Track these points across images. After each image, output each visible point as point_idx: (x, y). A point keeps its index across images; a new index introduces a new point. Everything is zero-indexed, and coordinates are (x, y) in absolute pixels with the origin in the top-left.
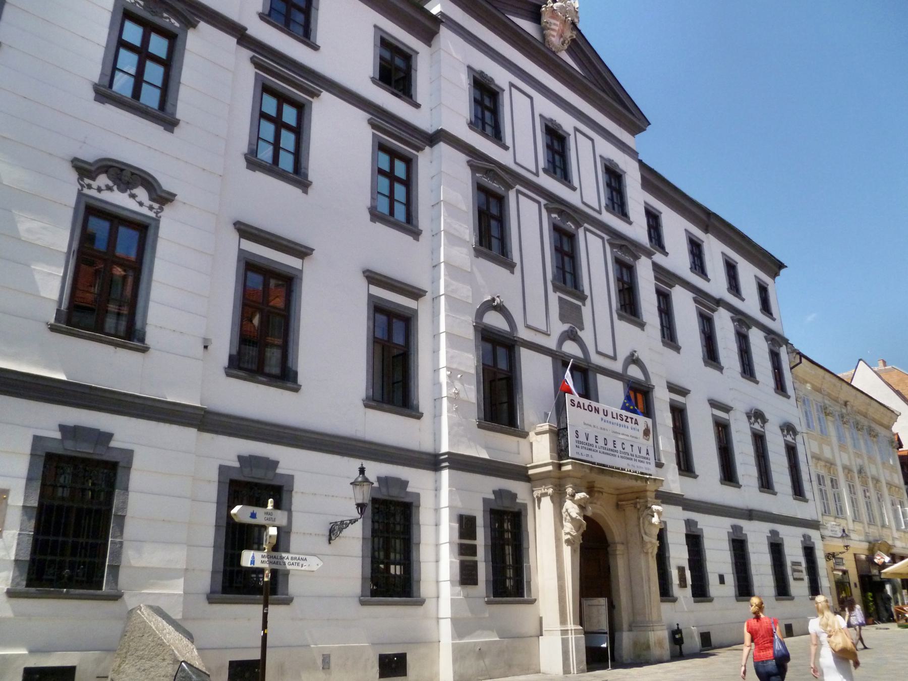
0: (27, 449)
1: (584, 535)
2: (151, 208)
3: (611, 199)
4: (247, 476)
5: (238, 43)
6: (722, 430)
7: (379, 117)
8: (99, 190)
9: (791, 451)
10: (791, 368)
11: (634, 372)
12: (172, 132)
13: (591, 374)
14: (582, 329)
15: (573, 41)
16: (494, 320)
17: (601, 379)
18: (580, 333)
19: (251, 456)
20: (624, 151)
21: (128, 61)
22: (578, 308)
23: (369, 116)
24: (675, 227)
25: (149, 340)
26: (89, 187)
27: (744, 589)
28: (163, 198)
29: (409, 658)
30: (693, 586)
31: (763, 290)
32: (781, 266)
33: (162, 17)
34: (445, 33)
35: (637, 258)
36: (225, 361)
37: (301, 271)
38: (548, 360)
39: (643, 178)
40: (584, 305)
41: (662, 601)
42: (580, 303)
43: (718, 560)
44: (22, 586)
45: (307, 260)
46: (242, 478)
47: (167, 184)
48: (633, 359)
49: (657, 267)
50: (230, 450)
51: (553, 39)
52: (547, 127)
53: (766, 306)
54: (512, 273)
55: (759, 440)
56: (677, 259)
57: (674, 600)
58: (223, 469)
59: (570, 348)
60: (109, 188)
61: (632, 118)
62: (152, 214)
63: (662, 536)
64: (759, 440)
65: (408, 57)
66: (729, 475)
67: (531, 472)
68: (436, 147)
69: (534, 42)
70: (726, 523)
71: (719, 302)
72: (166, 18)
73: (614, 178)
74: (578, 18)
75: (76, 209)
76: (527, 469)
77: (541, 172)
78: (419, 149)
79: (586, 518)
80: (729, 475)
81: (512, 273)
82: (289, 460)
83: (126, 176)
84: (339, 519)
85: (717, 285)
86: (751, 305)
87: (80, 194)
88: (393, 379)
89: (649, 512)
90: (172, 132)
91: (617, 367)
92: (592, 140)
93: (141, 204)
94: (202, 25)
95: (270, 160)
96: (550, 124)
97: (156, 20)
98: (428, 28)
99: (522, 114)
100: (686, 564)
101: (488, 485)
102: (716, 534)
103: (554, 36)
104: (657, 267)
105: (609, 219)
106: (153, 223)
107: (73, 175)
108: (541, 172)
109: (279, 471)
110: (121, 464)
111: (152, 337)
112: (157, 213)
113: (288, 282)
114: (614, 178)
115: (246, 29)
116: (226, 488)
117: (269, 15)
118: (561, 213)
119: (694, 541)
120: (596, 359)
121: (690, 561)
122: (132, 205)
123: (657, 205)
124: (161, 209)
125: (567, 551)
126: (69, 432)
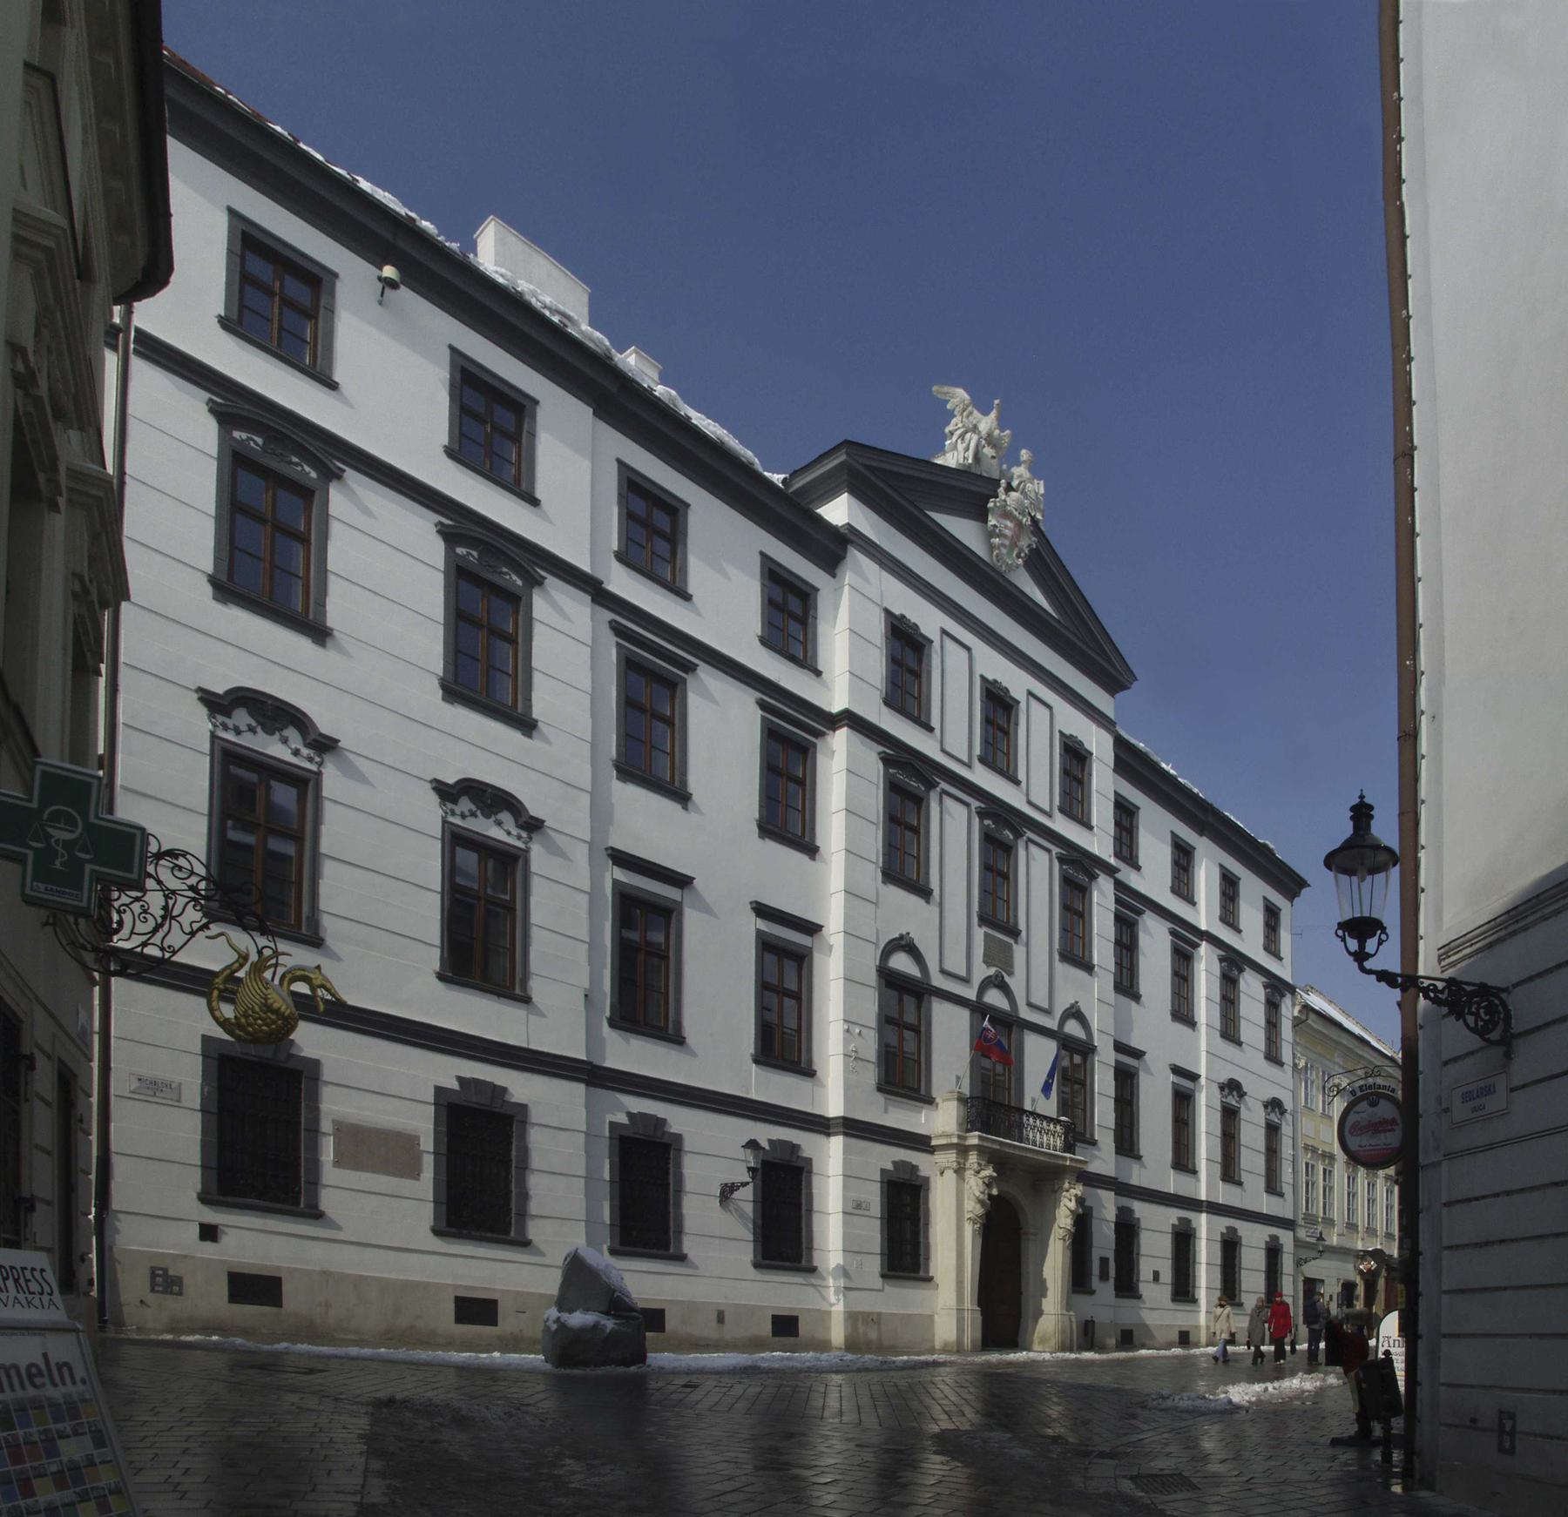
0: (197, 1047)
2: (519, 838)
3: (1065, 793)
7: (461, 526)
8: (238, 732)
9: (1272, 1130)
11: (1073, 1028)
14: (1011, 974)
18: (1007, 978)
22: (1009, 948)
23: (207, 395)
24: (1157, 830)
27: (1183, 1290)
34: (855, 557)
38: (965, 1014)
39: (1117, 758)
42: (1011, 941)
43: (1155, 1251)
44: (618, 1247)
45: (686, 891)
47: (325, 724)
48: (1075, 1013)
49: (1120, 886)
52: (988, 691)
57: (1092, 1292)
59: (994, 998)
60: (473, 814)
62: (314, 768)
64: (1230, 1116)
66: (1183, 1160)
67: (934, 1143)
70: (1172, 1215)
72: (297, 464)
73: (1074, 756)
76: (929, 1138)
79: (990, 1197)
80: (1229, 1171)
83: (276, 714)
85: (1204, 914)
91: (1052, 1024)
92: (968, 649)
93: (509, 833)
94: (351, 475)
98: (831, 548)
100: (1111, 1256)
102: (1156, 1225)
104: (1120, 886)
105: (1063, 826)
107: (434, 799)
114: (1074, 756)
117: (240, 321)
121: (1118, 1252)
122: (496, 833)
123: (1134, 795)
124: (530, 838)
125: (968, 1230)
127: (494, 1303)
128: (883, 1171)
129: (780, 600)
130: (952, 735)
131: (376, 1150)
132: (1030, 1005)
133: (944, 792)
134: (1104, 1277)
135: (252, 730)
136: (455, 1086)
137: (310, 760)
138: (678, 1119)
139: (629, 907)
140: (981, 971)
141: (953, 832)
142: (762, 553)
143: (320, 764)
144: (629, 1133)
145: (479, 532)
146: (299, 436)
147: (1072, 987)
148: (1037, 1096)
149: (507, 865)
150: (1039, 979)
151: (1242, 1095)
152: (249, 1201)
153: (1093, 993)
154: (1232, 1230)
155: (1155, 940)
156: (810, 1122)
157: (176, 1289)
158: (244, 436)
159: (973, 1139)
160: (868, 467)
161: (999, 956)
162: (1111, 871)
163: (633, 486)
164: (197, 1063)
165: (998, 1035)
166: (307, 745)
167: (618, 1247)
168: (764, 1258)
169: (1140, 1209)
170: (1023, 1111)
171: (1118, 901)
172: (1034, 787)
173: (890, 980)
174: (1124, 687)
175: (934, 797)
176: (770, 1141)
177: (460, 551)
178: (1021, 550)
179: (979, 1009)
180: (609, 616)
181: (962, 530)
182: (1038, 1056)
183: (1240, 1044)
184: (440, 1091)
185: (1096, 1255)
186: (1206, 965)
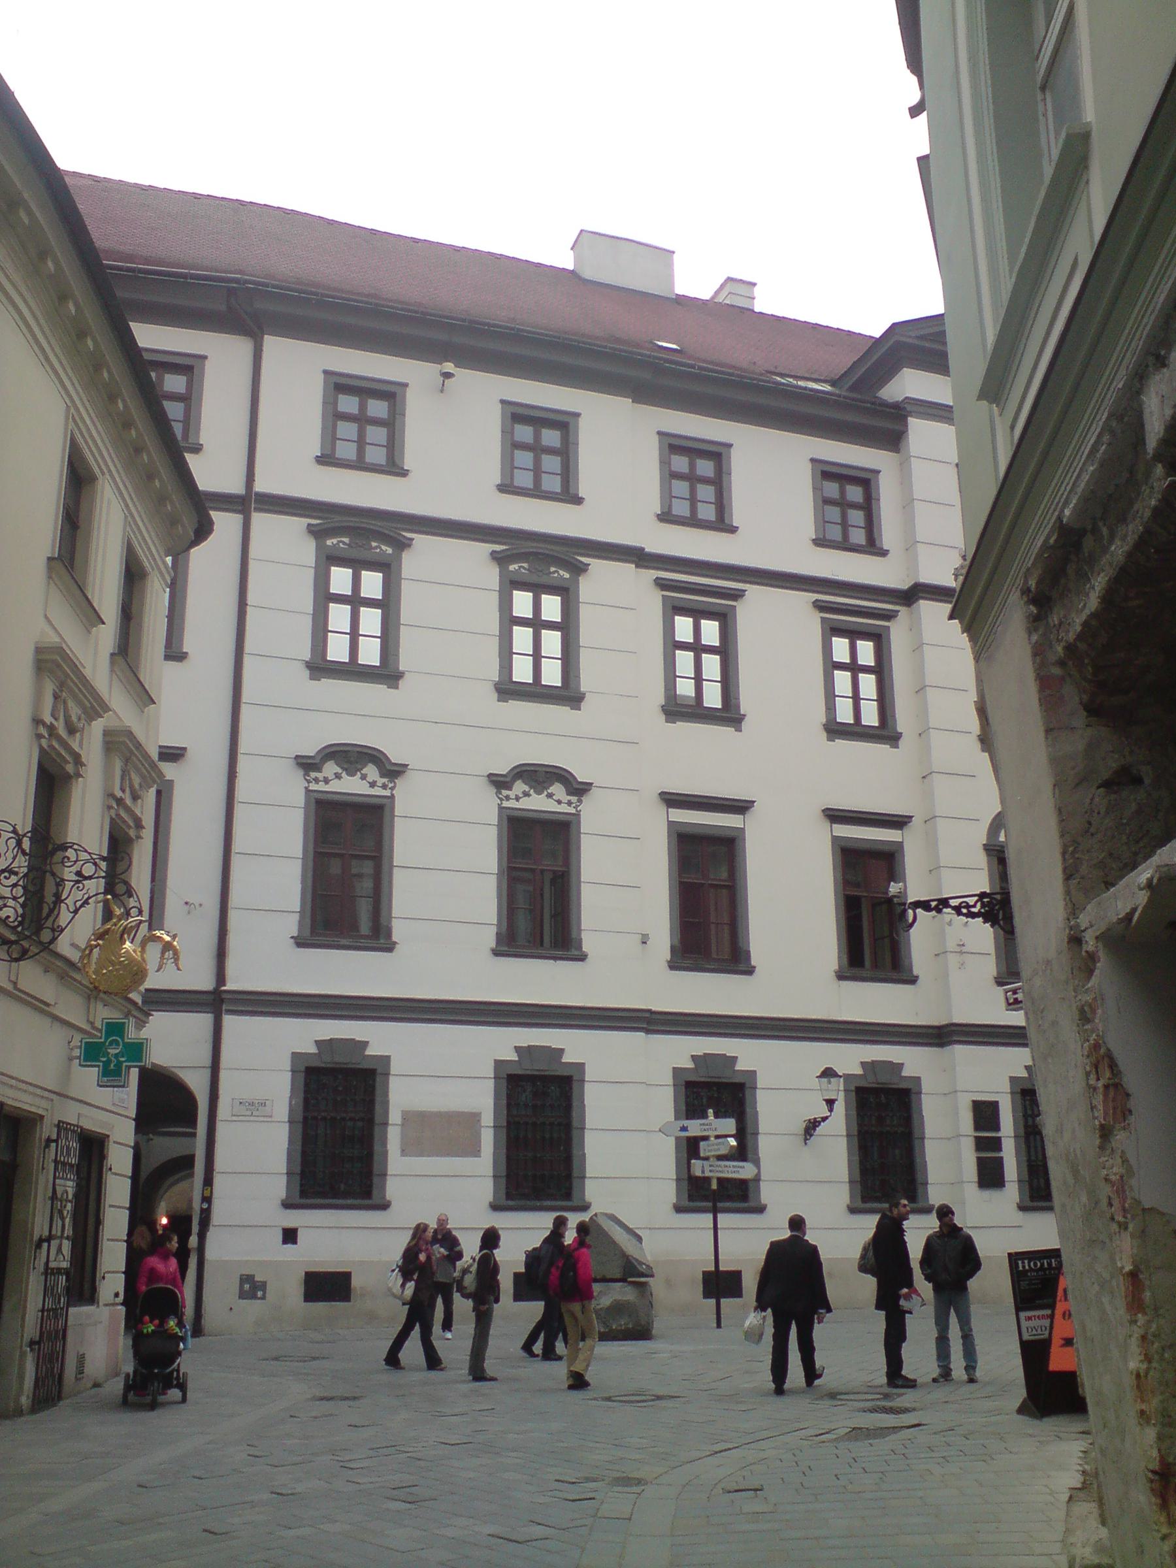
2: (569, 803)
4: (327, 1061)
5: (637, 567)
8: (326, 781)
12: (397, 688)
19: (873, 1062)
21: (684, 660)
25: (586, 948)
26: (508, 798)
28: (579, 790)
33: (371, 548)
34: (916, 425)
36: (667, 955)
37: (743, 830)
45: (905, 829)
47: (395, 756)
50: (683, 1051)
60: (526, 794)
62: (387, 793)
72: (554, 572)
78: (889, 616)
87: (501, 808)
90: (397, 688)
93: (559, 802)
97: (544, 580)
109: (739, 1067)
110: (379, 1071)
111: (589, 942)
113: (727, 848)
115: (643, 549)
116: (301, 1077)
124: (580, 801)
126: (870, 1067)
131: (444, 1133)
136: (691, 1065)
137: (384, 787)
142: (659, 433)
143: (392, 789)
145: (530, 547)
146: (375, 525)
152: (349, 1202)
157: (260, 1294)
158: (335, 541)
167: (686, 1203)
177: (512, 567)
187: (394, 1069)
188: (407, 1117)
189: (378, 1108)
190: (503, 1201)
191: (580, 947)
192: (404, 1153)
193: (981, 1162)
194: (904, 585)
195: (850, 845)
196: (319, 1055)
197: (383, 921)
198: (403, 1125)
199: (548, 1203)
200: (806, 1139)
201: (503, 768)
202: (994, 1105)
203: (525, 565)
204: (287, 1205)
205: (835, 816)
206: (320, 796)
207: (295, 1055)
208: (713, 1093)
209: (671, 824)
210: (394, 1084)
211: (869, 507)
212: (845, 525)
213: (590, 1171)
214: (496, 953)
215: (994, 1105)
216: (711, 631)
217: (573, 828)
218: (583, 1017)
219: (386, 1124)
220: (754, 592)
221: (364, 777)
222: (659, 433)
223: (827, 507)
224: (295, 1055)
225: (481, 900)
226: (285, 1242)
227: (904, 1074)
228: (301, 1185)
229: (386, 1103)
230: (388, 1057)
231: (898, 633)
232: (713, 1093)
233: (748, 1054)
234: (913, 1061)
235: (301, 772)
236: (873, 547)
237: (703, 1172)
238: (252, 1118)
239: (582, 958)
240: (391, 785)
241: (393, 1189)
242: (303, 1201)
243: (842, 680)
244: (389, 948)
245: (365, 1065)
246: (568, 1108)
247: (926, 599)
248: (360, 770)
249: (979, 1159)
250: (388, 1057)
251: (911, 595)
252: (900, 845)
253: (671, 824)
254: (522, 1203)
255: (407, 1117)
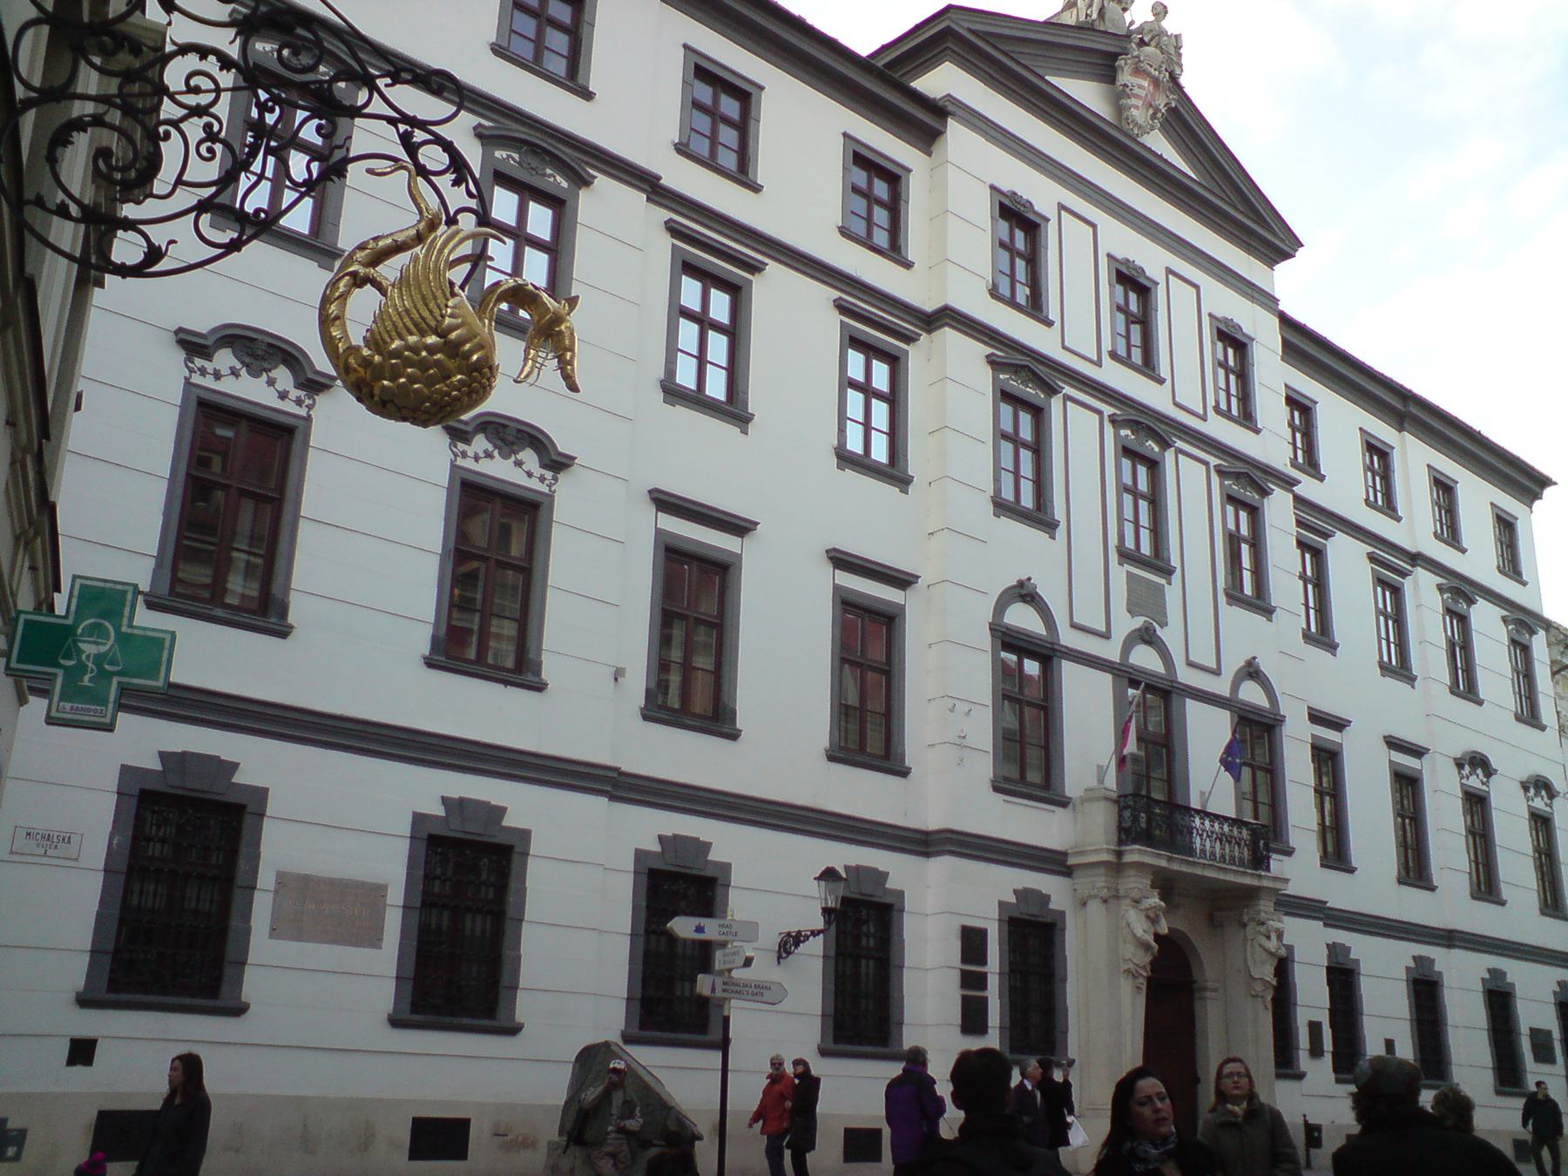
0: (406, 830)
1: (1154, 964)
2: (542, 479)
4: (454, 830)
5: (649, 199)
6: (1407, 786)
8: (217, 376)
10: (1554, 674)
11: (1251, 694)
13: (1175, 699)
14: (1163, 624)
15: (1173, 111)
16: (1022, 618)
17: (1193, 708)
18: (1159, 632)
20: (1252, 299)
22: (1160, 590)
24: (1342, 423)
25: (546, 675)
26: (464, 455)
28: (557, 463)
29: (1534, 1026)
30: (1334, 1054)
31: (1506, 526)
32: (1543, 482)
34: (955, 131)
35: (1265, 493)
36: (640, 700)
38: (1107, 679)
39: (1285, 342)
40: (1169, 583)
41: (1279, 1076)
42: (1163, 581)
46: (163, 789)
48: (1251, 671)
50: (648, 827)
51: (1134, 112)
53: (1511, 564)
54: (1053, 537)
55: (1476, 803)
56: (1342, 485)
57: (1300, 1076)
58: (640, 855)
59: (1145, 659)
60: (489, 455)
61: (1270, 237)
62: (302, 412)
63: (1283, 967)
64: (1476, 803)
65: (894, 177)
68: (936, 334)
69: (1101, 125)
70: (1404, 953)
71: (1416, 559)
74: (1181, 66)
75: (450, 489)
77: (1106, 358)
78: (909, 339)
79: (1157, 937)
81: (1053, 537)
82: (727, 842)
84: (794, 929)
86: (1478, 559)
87: (454, 467)
88: (868, 724)
89: (1262, 929)
91: (1221, 686)
93: (530, 475)
95: (693, 386)
96: (1125, 270)
99: (1076, 258)
100: (1324, 1018)
101: (1006, 882)
103: (1137, 108)
106: (545, 500)
108: (1106, 358)
109: (712, 857)
110: (249, 809)
111: (551, 668)
112: (550, 486)
118: (1135, 425)
119: (1342, 978)
120: (1186, 676)
121: (1333, 1012)
124: (556, 479)
126: (455, 806)
127: (465, 1123)
128: (1002, 904)
129: (863, 184)
130: (1077, 325)
131: (333, 910)
132: (1191, 664)
133: (1067, 398)
134: (1316, 1051)
135: (235, 373)
136: (157, 766)
138: (521, 805)
139: (676, 560)
140: (1125, 624)
141: (1081, 439)
143: (310, 407)
144: (659, 865)
145: (520, 132)
147: (1245, 634)
148: (1210, 784)
149: (718, 573)
150: (1203, 633)
151: (1489, 772)
152: (152, 998)
153: (1274, 640)
154: (1496, 974)
155: (1347, 561)
156: (297, 724)
159: (1136, 854)
160: (970, 30)
161: (1146, 602)
162: (1288, 483)
163: (703, 71)
164: (402, 848)
165: (1154, 703)
166: (298, 386)
167: (636, 1032)
168: (836, 1040)
169: (1361, 947)
170: (1188, 810)
171: (1300, 523)
172: (1185, 382)
173: (1008, 640)
174: (1287, 256)
175: (1056, 403)
176: (847, 868)
178: (1157, 110)
179: (1126, 675)
180: (666, 215)
181: (1085, 92)
182: (1206, 734)
183: (1480, 703)
184: (419, 819)
185: (1302, 1018)
186: (1423, 591)
187: (534, 849)
188: (282, 879)
189: (242, 864)
190: (407, 1015)
191: (538, 673)
192: (274, 932)
193: (966, 1001)
194: (930, 307)
195: (852, 598)
196: (445, 819)
197: (276, 590)
198: (276, 892)
199: (466, 1021)
200: (780, 957)
201: (202, 323)
202: (982, 933)
203: (516, 156)
204: (85, 1001)
205: (841, 560)
206: (204, 395)
207: (125, 769)
208: (676, 888)
209: (659, 532)
210: (269, 829)
211: (895, 207)
212: (539, 44)
213: (523, 982)
214: (430, 664)
215: (982, 933)
216: (881, 376)
217: (298, 437)
218: (537, 768)
219: (1001, 974)
220: (774, 269)
221: (271, 382)
222: (845, 135)
223: (517, 14)
224: (125, 769)
225: (416, 586)
226: (72, 1061)
227: (505, 823)
228: (112, 971)
229: (256, 857)
230: (265, 791)
231: (917, 357)
232: (676, 888)
233: (727, 842)
234: (898, 869)
235: (182, 355)
236: (895, 251)
237: (713, 990)
238: (44, 860)
239: (540, 687)
240: (308, 402)
241: (254, 984)
242: (113, 997)
243: (688, 332)
244: (282, 631)
245: (232, 798)
246: (232, 854)
247: (951, 326)
248: (267, 370)
249: (965, 999)
250: (265, 791)
251: (932, 320)
252: (902, 608)
253: (659, 532)
254: (432, 1018)
255: (282, 879)
